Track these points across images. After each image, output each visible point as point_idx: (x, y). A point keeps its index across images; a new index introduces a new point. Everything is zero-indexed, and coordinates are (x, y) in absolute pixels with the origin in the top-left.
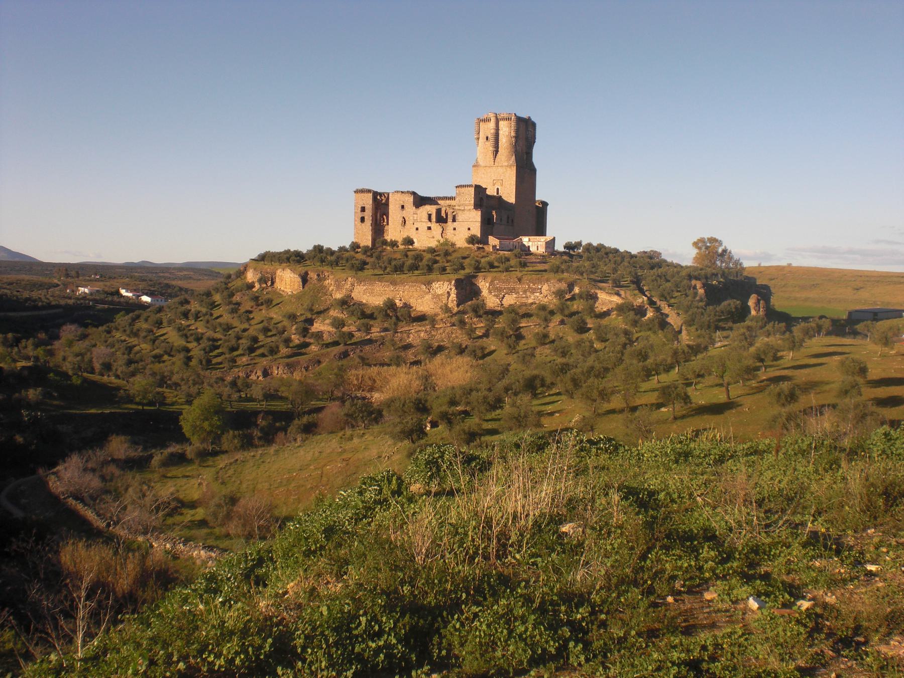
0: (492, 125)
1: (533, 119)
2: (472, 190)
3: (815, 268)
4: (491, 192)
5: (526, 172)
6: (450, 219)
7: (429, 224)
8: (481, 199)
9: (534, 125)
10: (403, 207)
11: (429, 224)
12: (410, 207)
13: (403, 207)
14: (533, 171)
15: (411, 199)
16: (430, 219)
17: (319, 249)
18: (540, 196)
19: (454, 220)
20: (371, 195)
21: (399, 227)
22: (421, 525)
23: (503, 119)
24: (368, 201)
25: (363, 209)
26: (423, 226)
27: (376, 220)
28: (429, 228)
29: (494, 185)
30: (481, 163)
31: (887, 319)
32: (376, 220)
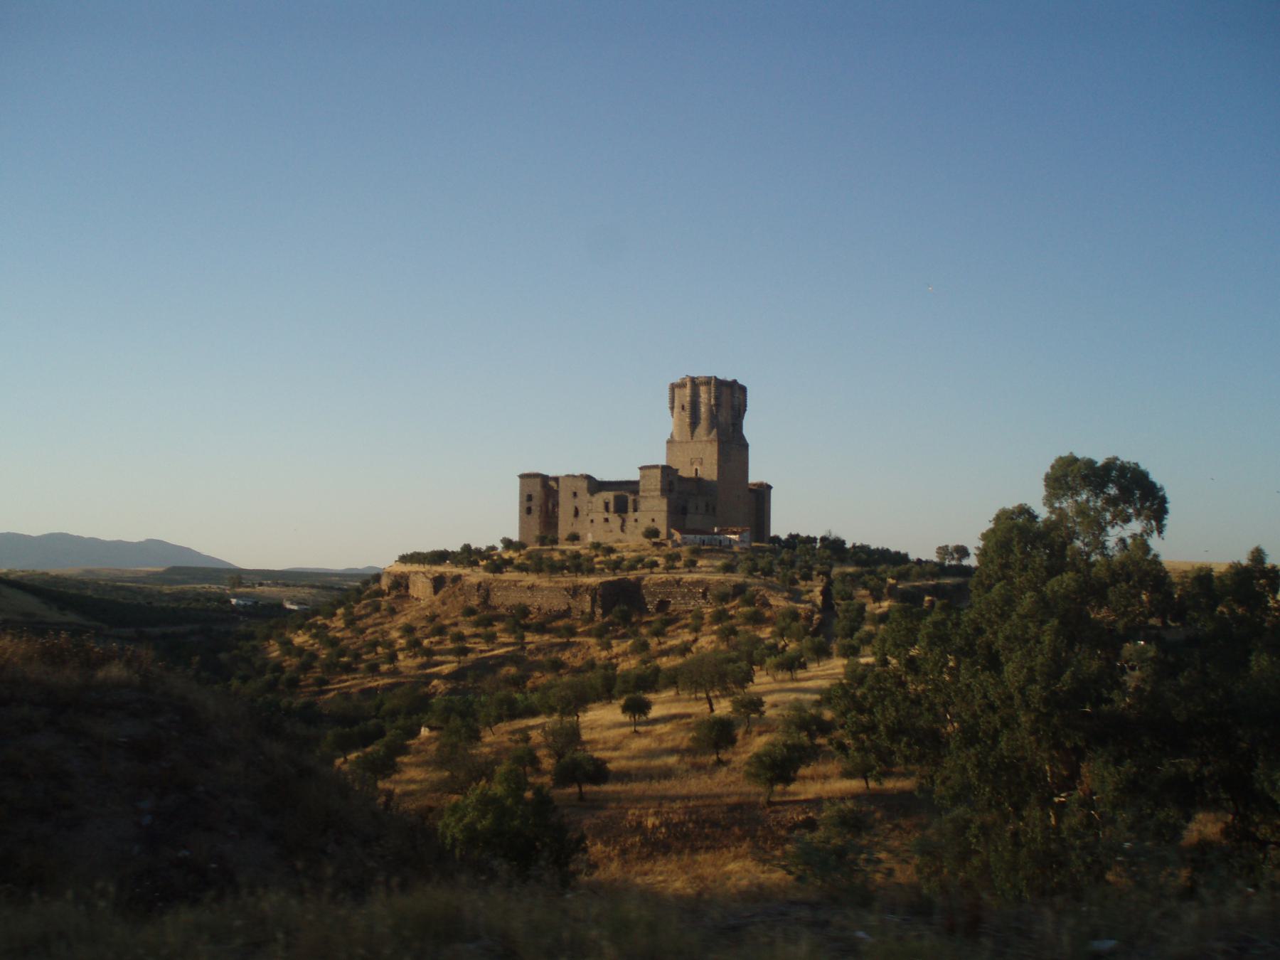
0: (688, 391)
1: (740, 382)
2: (658, 472)
3: (79, 537)
4: (687, 472)
5: (733, 447)
6: (630, 508)
7: (606, 515)
8: (671, 483)
9: (743, 389)
10: (575, 494)
11: (606, 515)
12: (584, 496)
13: (575, 494)
14: (744, 446)
15: (584, 484)
16: (607, 509)
17: (467, 548)
18: (754, 477)
19: (635, 510)
20: (538, 480)
21: (572, 519)
22: (878, 611)
23: (702, 384)
24: (537, 489)
25: (530, 498)
26: (599, 517)
27: (547, 512)
28: (606, 520)
29: (692, 464)
30: (677, 438)
31: (574, 476)
32: (547, 512)
